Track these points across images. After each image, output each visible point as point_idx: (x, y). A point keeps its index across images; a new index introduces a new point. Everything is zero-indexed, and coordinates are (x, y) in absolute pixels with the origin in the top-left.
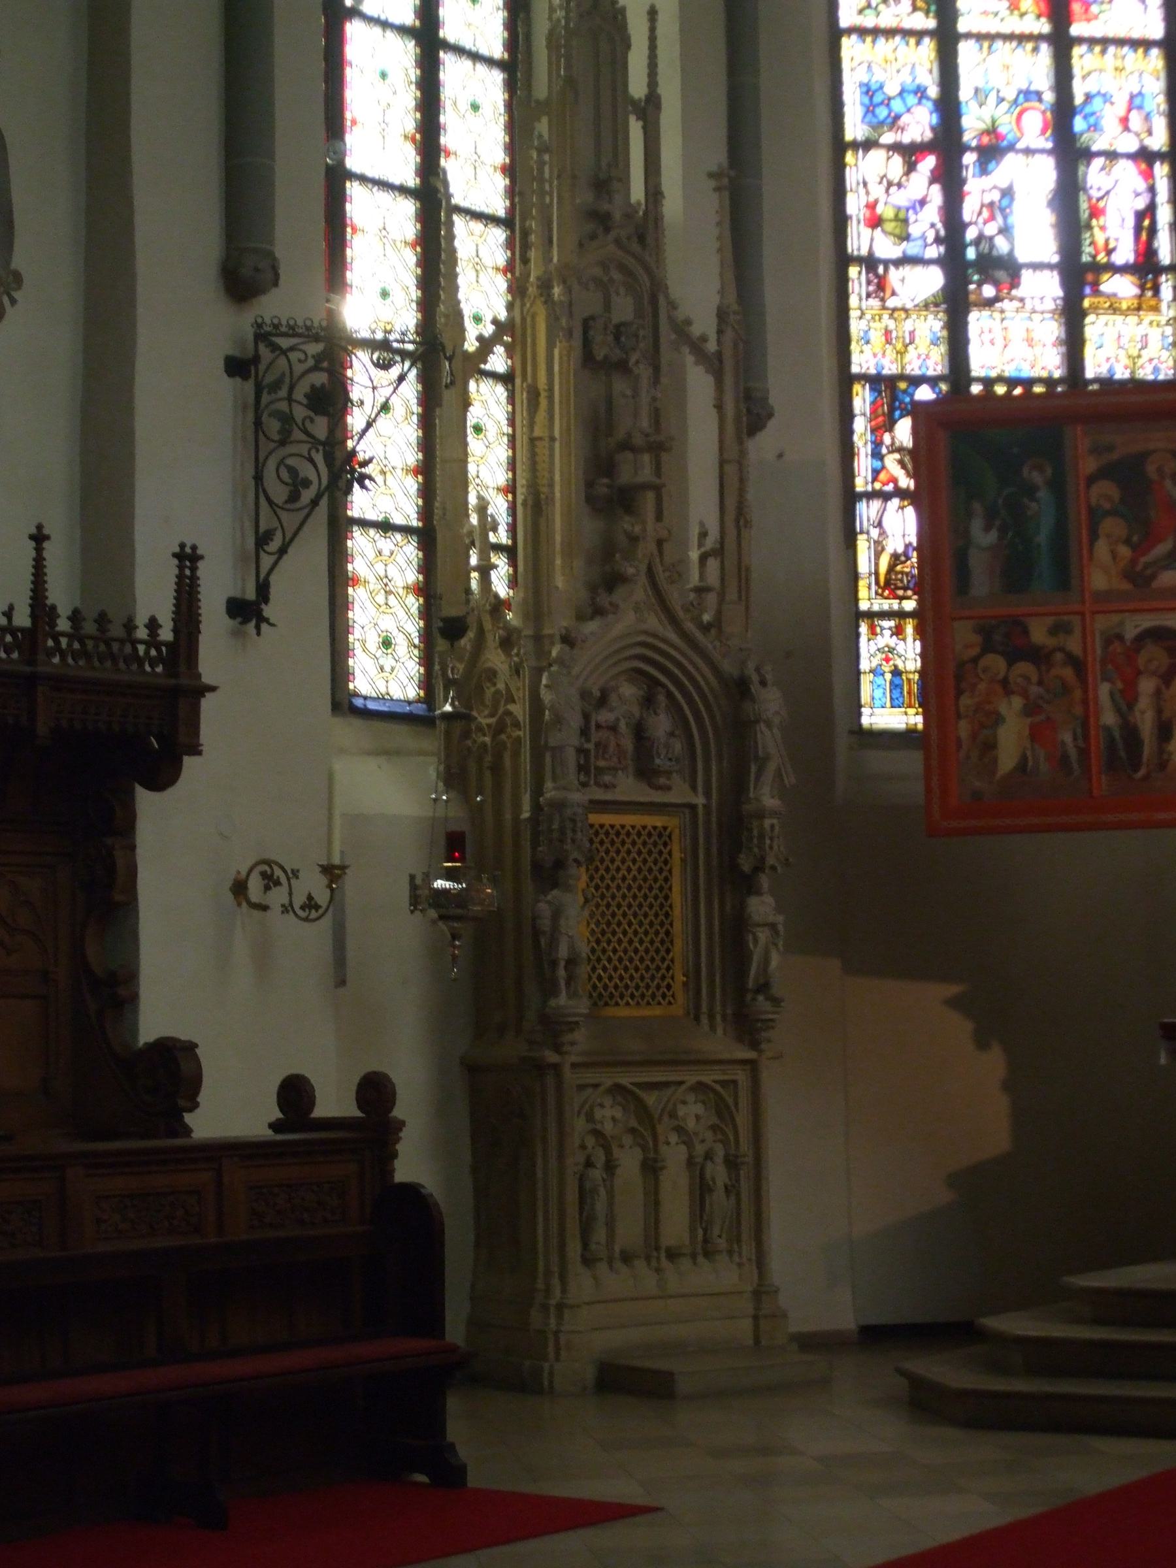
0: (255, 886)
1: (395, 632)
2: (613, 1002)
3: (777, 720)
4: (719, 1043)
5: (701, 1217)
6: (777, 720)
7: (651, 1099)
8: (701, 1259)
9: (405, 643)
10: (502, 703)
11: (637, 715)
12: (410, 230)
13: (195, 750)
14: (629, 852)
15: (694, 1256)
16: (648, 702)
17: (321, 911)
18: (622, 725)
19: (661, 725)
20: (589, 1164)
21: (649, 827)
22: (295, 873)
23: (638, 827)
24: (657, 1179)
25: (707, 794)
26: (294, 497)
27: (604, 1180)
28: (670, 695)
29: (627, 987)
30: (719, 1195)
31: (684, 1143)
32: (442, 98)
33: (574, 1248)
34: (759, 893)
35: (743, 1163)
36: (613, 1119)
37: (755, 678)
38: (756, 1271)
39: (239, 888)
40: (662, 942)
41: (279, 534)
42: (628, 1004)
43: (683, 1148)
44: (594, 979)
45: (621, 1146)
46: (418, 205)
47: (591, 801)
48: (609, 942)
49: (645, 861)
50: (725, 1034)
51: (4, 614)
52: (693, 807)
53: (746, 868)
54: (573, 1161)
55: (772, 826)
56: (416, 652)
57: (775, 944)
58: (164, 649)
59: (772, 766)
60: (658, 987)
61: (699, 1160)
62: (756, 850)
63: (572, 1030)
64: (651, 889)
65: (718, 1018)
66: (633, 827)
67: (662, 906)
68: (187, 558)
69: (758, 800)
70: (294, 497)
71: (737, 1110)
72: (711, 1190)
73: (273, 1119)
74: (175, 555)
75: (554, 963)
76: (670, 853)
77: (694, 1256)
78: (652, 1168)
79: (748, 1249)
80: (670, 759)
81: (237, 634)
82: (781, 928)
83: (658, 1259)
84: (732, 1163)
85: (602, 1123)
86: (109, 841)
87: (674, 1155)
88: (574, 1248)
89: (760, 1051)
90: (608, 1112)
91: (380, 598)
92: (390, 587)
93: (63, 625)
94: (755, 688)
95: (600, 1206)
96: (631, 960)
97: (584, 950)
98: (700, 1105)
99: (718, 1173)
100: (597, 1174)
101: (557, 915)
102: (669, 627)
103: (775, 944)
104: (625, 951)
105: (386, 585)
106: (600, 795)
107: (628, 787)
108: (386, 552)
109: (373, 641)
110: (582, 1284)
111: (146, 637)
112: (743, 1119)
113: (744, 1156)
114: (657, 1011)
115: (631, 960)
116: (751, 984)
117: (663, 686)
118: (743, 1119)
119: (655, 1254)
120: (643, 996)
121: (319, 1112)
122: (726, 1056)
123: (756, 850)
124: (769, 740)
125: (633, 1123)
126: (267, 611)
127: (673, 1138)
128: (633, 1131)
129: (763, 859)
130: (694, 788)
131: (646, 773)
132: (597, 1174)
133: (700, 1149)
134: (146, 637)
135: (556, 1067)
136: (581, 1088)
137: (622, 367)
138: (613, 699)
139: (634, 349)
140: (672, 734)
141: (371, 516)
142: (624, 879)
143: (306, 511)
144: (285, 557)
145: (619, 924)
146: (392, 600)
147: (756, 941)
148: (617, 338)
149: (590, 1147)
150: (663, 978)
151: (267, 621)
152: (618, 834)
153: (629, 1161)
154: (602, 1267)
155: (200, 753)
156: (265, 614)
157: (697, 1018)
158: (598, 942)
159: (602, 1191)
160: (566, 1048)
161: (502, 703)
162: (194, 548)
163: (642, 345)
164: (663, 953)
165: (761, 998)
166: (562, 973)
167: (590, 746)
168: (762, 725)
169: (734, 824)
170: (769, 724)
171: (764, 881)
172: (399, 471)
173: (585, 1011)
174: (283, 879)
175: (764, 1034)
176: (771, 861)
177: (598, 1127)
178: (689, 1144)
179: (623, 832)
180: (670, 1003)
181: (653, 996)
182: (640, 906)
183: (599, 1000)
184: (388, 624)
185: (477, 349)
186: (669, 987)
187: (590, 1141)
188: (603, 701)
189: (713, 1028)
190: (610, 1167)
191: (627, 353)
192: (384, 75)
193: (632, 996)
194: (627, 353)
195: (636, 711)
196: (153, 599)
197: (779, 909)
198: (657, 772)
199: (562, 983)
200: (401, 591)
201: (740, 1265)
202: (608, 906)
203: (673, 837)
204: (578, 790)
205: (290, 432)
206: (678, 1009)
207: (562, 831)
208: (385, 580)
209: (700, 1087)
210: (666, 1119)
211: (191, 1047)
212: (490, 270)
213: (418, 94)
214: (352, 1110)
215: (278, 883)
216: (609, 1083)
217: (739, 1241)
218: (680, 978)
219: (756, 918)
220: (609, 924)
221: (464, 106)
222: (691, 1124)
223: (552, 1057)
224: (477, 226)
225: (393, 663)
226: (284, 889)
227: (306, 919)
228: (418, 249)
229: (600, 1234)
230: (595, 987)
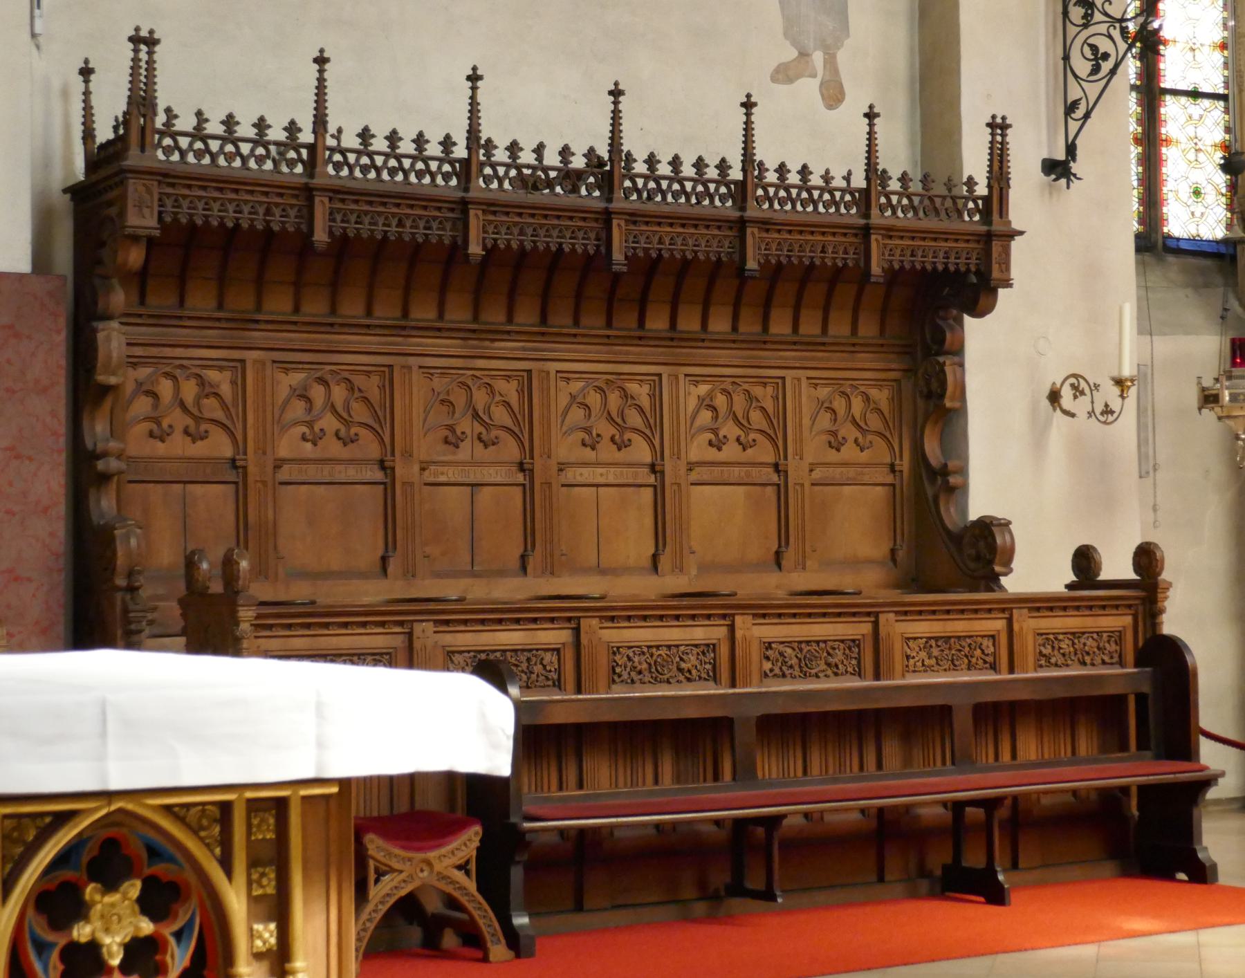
0: (1066, 393)
1: (1204, 183)
9: (1214, 192)
13: (1007, 283)
17: (1115, 415)
22: (1097, 386)
26: (1096, 69)
39: (1054, 397)
41: (1083, 102)
51: (844, 178)
56: (1224, 199)
58: (980, 202)
68: (998, 127)
70: (1096, 69)
73: (1068, 581)
74: (988, 125)
81: (1051, 190)
86: (941, 359)
91: (1191, 156)
92: (1200, 145)
93: (894, 185)
108: (1196, 117)
109: (1185, 192)
111: (776, 181)
121: (1104, 575)
126: (1075, 167)
134: (776, 181)
143: (1105, 81)
144: (1089, 121)
146: (1201, 156)
151: (1075, 175)
155: (1010, 286)
156: (1073, 171)
162: (1004, 118)
174: (1087, 390)
184: (1198, 177)
196: (974, 163)
200: (1209, 149)
205: (1092, 15)
211: (1006, 525)
214: (1129, 574)
215: (1082, 393)
225: (1203, 210)
226: (1087, 399)
227: (1105, 423)
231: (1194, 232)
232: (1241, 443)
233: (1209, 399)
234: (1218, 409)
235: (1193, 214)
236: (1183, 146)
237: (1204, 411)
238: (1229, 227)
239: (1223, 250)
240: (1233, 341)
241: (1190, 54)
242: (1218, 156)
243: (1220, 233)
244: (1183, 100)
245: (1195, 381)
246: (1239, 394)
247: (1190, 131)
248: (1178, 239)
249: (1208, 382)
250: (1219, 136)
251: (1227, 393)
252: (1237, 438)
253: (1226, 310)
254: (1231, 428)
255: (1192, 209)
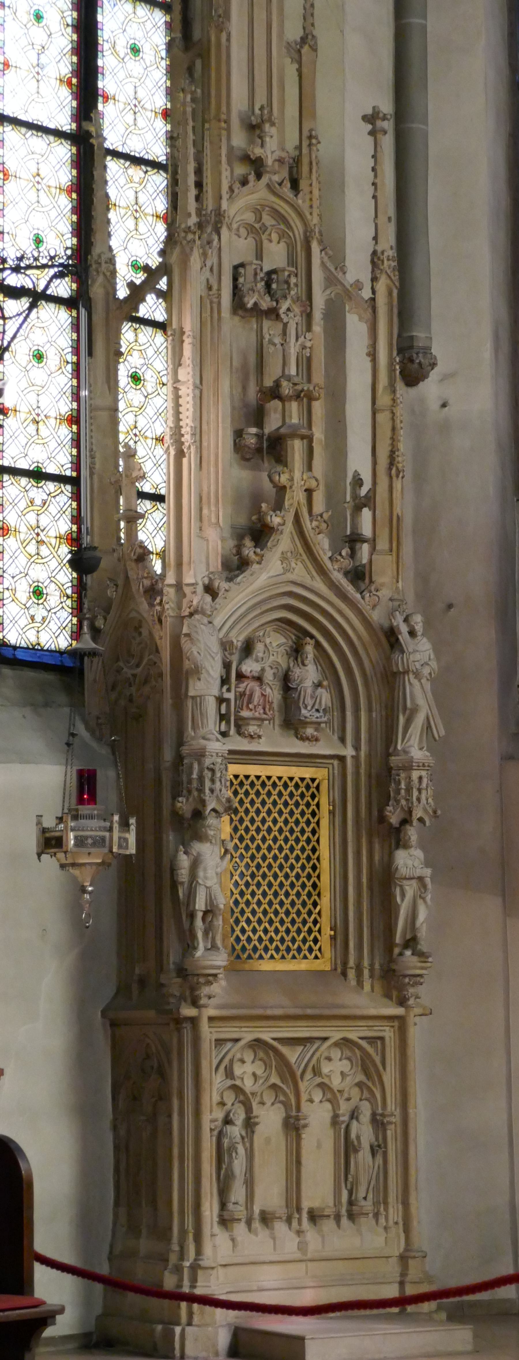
2: (257, 955)
3: (426, 671)
4: (367, 1000)
5: (346, 1179)
6: (426, 671)
7: (292, 1055)
8: (345, 1221)
10: (147, 654)
11: (284, 666)
12: (66, 176)
14: (275, 803)
15: (338, 1218)
16: (296, 652)
18: (269, 676)
19: (308, 674)
20: (227, 1121)
21: (296, 779)
23: (285, 778)
24: (299, 1137)
25: (357, 748)
27: (243, 1138)
28: (318, 645)
29: (271, 940)
30: (364, 1156)
31: (329, 1100)
32: (100, 42)
33: (210, 1209)
34: (406, 846)
35: (391, 1123)
36: (254, 1075)
37: (404, 629)
38: (402, 1236)
40: (309, 895)
42: (272, 957)
43: (328, 1106)
44: (238, 932)
45: (263, 1103)
46: (74, 150)
47: (231, 752)
48: (253, 894)
49: (292, 813)
50: (373, 990)
52: (342, 759)
53: (394, 820)
54: (211, 1116)
55: (420, 778)
56: (69, 602)
57: (424, 899)
59: (420, 720)
60: (304, 941)
61: (346, 1118)
62: (403, 802)
63: (209, 983)
64: (297, 840)
65: (366, 973)
66: (280, 778)
67: (308, 859)
69: (405, 752)
71: (384, 1068)
72: (356, 1151)
75: (192, 916)
76: (318, 805)
77: (338, 1218)
78: (293, 1126)
79: (394, 1212)
80: (317, 711)
82: (428, 880)
83: (300, 1221)
84: (378, 1123)
85: (242, 1079)
87: (317, 1115)
88: (210, 1209)
89: (407, 1008)
90: (249, 1068)
91: (32, 548)
92: (42, 536)
94: (404, 636)
95: (239, 1165)
96: (276, 913)
97: (222, 901)
98: (346, 1062)
99: (364, 1131)
100: (236, 1131)
101: (195, 864)
102: (318, 578)
103: (424, 899)
104: (270, 903)
105: (38, 535)
106: (244, 745)
107: (273, 739)
108: (38, 502)
110: (217, 1245)
112: (390, 1077)
113: (392, 1115)
114: (303, 965)
115: (276, 913)
116: (398, 939)
117: (312, 637)
118: (390, 1077)
119: (297, 1216)
120: (288, 950)
122: (373, 1012)
123: (403, 802)
124: (418, 693)
125: (275, 1079)
127: (318, 1095)
128: (274, 1086)
129: (410, 812)
130: (343, 740)
131: (291, 722)
132: (236, 1131)
133: (344, 1108)
135: (194, 1021)
136: (220, 1042)
137: (273, 313)
138: (259, 648)
139: (285, 297)
140: (319, 685)
141: (23, 464)
142: (269, 830)
145: (264, 876)
146: (44, 551)
147: (403, 895)
148: (268, 286)
149: (230, 1104)
150: (310, 931)
152: (263, 785)
153: (270, 1119)
154: (240, 1229)
157: (344, 974)
158: (242, 894)
159: (241, 1149)
160: (203, 1001)
161: (147, 654)
163: (293, 293)
164: (310, 906)
165: (408, 953)
166: (199, 923)
167: (231, 696)
168: (411, 676)
169: (383, 777)
170: (417, 675)
171: (412, 833)
172: (52, 421)
173: (224, 963)
175: (411, 990)
176: (418, 813)
177: (238, 1083)
178: (333, 1102)
179: (269, 783)
180: (316, 957)
181: (299, 950)
182: (286, 858)
183: (239, 955)
184: (39, 573)
185: (150, 293)
186: (316, 941)
187: (229, 1098)
188: (248, 649)
189: (360, 983)
190: (250, 1124)
191: (277, 302)
192: (39, 17)
193: (277, 949)
194: (277, 302)
195: (283, 661)
197: (427, 864)
198: (305, 724)
199: (200, 935)
200: (53, 541)
201: (386, 1228)
202: (253, 858)
203: (321, 788)
204: (218, 740)
206: (324, 965)
207: (201, 779)
208: (37, 529)
209: (346, 1043)
210: (309, 1075)
212: (150, 218)
213: (75, 37)
216: (248, 1037)
217: (386, 1203)
218: (327, 932)
219: (403, 871)
220: (253, 876)
221: (122, 49)
222: (336, 1082)
223: (188, 1011)
224: (136, 172)
228: (74, 196)
229: (238, 1193)
230: (238, 940)
231: (33, 640)
232: (87, 896)
233: (50, 842)
234: (61, 855)
235: (32, 618)
236: (22, 536)
237: (44, 856)
238: (76, 634)
239: (68, 662)
240: (80, 773)
241: (32, 428)
242: (65, 551)
243: (63, 642)
244: (24, 481)
245: (35, 820)
246: (87, 838)
247: (31, 518)
248: (15, 648)
249: (49, 822)
250: (65, 526)
251: (72, 835)
252: (83, 890)
253: (73, 735)
254: (74, 878)
255: (32, 612)
